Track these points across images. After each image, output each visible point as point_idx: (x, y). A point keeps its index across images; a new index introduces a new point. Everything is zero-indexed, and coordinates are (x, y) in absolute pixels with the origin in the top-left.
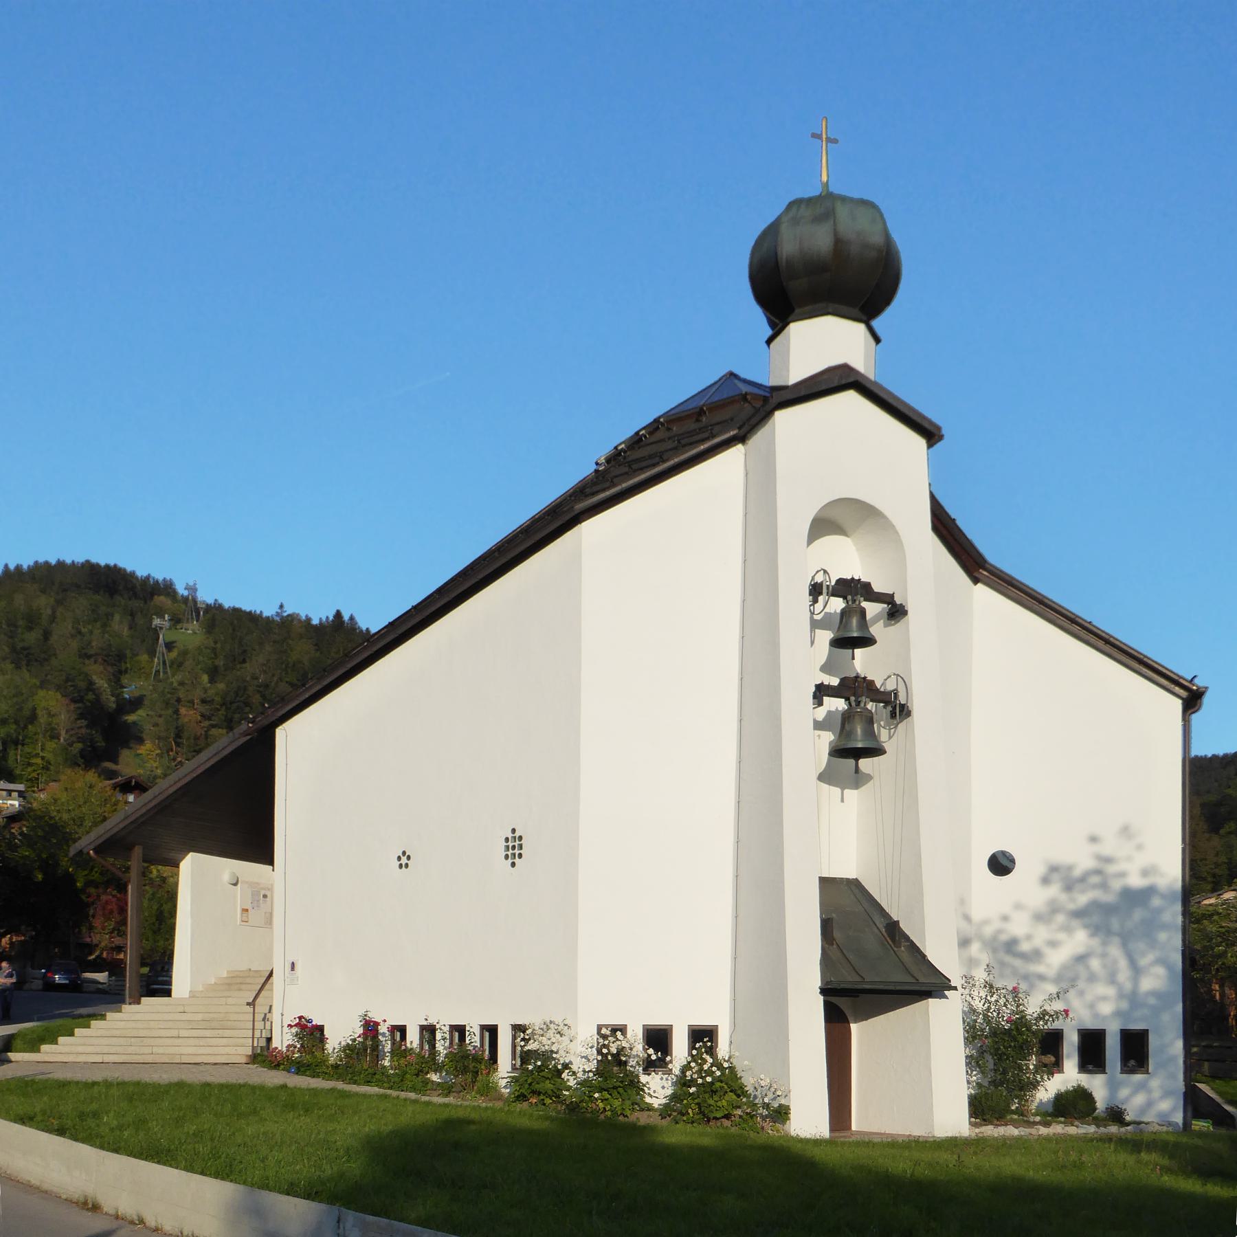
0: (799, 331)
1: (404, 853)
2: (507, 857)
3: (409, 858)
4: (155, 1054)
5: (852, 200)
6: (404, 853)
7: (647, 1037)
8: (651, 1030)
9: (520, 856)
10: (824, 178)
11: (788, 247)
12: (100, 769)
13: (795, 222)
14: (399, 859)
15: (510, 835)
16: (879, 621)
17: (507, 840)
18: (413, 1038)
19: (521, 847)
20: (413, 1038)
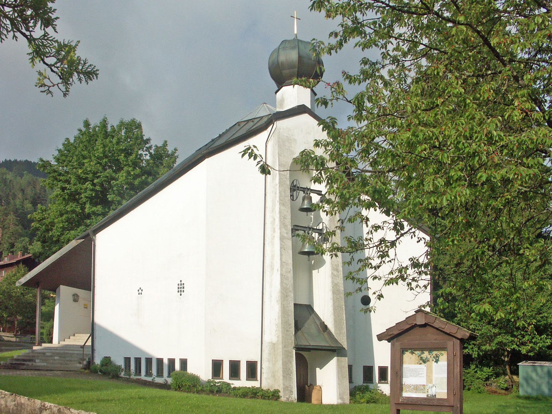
0: (286, 90)
1: (140, 288)
2: (178, 291)
3: (138, 291)
4: (454, 358)
5: (304, 42)
6: (140, 288)
7: (231, 365)
8: (462, 364)
9: (183, 291)
10: (296, 32)
11: (282, 58)
12: (365, 384)
13: (284, 48)
14: (138, 291)
15: (180, 283)
16: (311, 106)
17: (178, 285)
18: (177, 367)
19: (183, 288)
20: (177, 367)
